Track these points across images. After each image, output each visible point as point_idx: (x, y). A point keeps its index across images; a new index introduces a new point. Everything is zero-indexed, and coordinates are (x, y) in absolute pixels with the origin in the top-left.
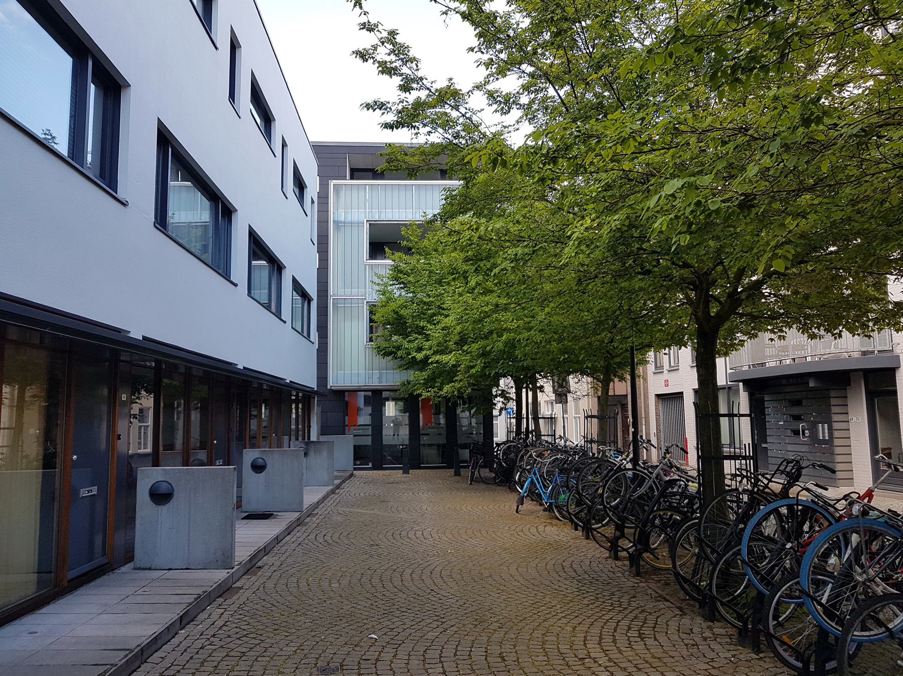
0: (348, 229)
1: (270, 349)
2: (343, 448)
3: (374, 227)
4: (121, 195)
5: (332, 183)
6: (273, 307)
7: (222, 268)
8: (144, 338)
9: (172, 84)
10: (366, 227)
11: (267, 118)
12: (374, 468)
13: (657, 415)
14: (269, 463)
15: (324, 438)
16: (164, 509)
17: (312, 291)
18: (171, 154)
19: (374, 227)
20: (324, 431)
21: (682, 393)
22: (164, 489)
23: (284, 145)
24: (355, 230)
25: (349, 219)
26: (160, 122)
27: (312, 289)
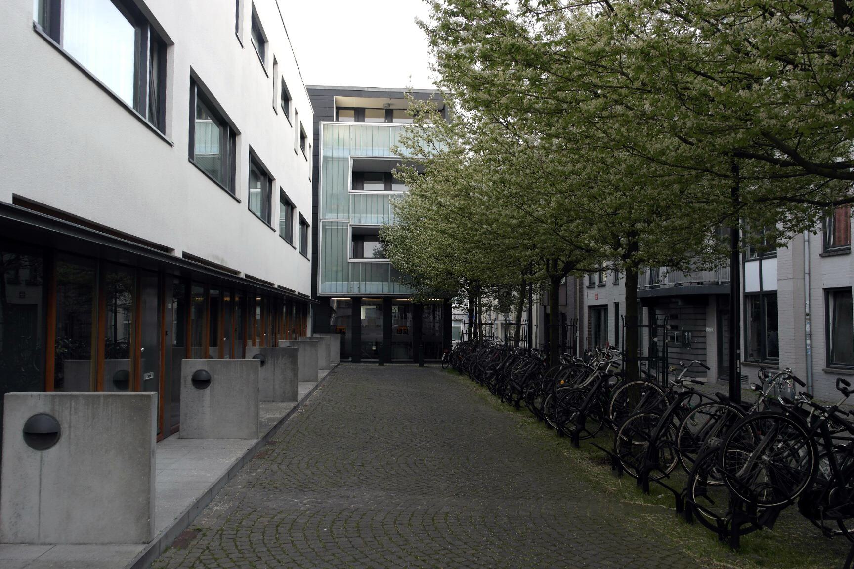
0: (335, 164)
1: (284, 267)
2: (331, 346)
3: (356, 161)
4: (237, 196)
5: (323, 123)
6: (266, 217)
7: (229, 187)
8: (17, 199)
9: (203, 47)
10: (350, 162)
11: (261, 39)
12: (353, 361)
13: (589, 323)
14: (216, 378)
15: (316, 335)
16: (53, 453)
17: (309, 220)
18: (204, 102)
19: (356, 161)
20: (314, 331)
21: (851, 288)
22: (203, 377)
23: (275, 62)
24: (341, 163)
25: (335, 155)
26: (192, 70)
27: (309, 219)
